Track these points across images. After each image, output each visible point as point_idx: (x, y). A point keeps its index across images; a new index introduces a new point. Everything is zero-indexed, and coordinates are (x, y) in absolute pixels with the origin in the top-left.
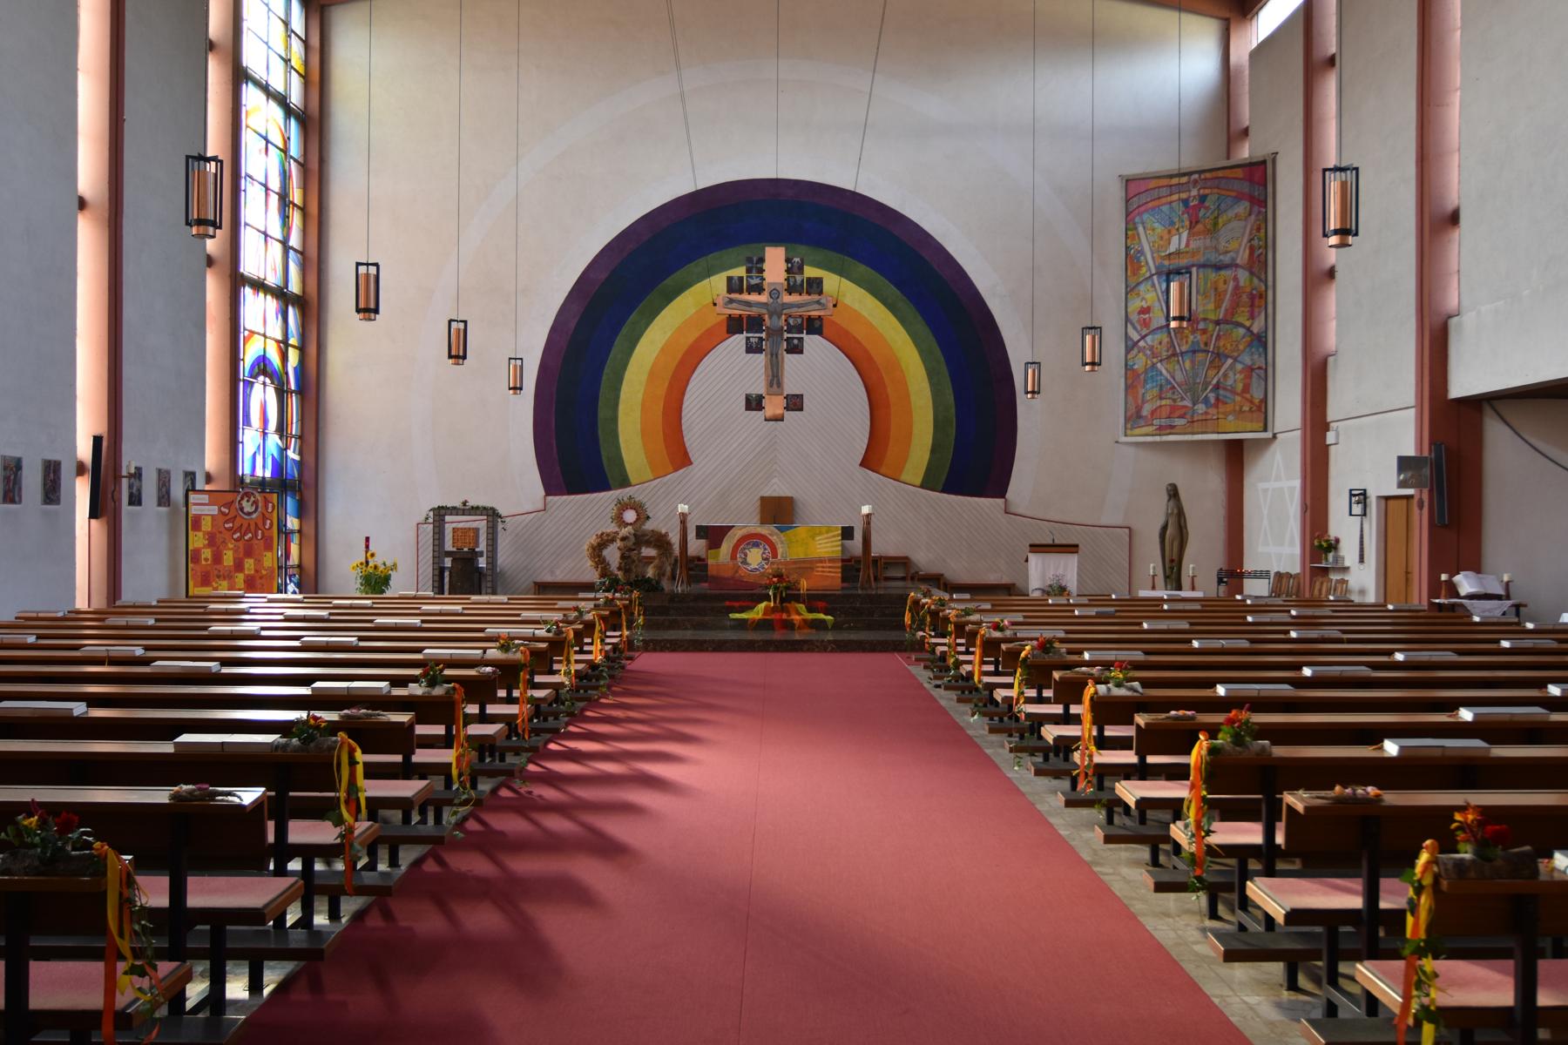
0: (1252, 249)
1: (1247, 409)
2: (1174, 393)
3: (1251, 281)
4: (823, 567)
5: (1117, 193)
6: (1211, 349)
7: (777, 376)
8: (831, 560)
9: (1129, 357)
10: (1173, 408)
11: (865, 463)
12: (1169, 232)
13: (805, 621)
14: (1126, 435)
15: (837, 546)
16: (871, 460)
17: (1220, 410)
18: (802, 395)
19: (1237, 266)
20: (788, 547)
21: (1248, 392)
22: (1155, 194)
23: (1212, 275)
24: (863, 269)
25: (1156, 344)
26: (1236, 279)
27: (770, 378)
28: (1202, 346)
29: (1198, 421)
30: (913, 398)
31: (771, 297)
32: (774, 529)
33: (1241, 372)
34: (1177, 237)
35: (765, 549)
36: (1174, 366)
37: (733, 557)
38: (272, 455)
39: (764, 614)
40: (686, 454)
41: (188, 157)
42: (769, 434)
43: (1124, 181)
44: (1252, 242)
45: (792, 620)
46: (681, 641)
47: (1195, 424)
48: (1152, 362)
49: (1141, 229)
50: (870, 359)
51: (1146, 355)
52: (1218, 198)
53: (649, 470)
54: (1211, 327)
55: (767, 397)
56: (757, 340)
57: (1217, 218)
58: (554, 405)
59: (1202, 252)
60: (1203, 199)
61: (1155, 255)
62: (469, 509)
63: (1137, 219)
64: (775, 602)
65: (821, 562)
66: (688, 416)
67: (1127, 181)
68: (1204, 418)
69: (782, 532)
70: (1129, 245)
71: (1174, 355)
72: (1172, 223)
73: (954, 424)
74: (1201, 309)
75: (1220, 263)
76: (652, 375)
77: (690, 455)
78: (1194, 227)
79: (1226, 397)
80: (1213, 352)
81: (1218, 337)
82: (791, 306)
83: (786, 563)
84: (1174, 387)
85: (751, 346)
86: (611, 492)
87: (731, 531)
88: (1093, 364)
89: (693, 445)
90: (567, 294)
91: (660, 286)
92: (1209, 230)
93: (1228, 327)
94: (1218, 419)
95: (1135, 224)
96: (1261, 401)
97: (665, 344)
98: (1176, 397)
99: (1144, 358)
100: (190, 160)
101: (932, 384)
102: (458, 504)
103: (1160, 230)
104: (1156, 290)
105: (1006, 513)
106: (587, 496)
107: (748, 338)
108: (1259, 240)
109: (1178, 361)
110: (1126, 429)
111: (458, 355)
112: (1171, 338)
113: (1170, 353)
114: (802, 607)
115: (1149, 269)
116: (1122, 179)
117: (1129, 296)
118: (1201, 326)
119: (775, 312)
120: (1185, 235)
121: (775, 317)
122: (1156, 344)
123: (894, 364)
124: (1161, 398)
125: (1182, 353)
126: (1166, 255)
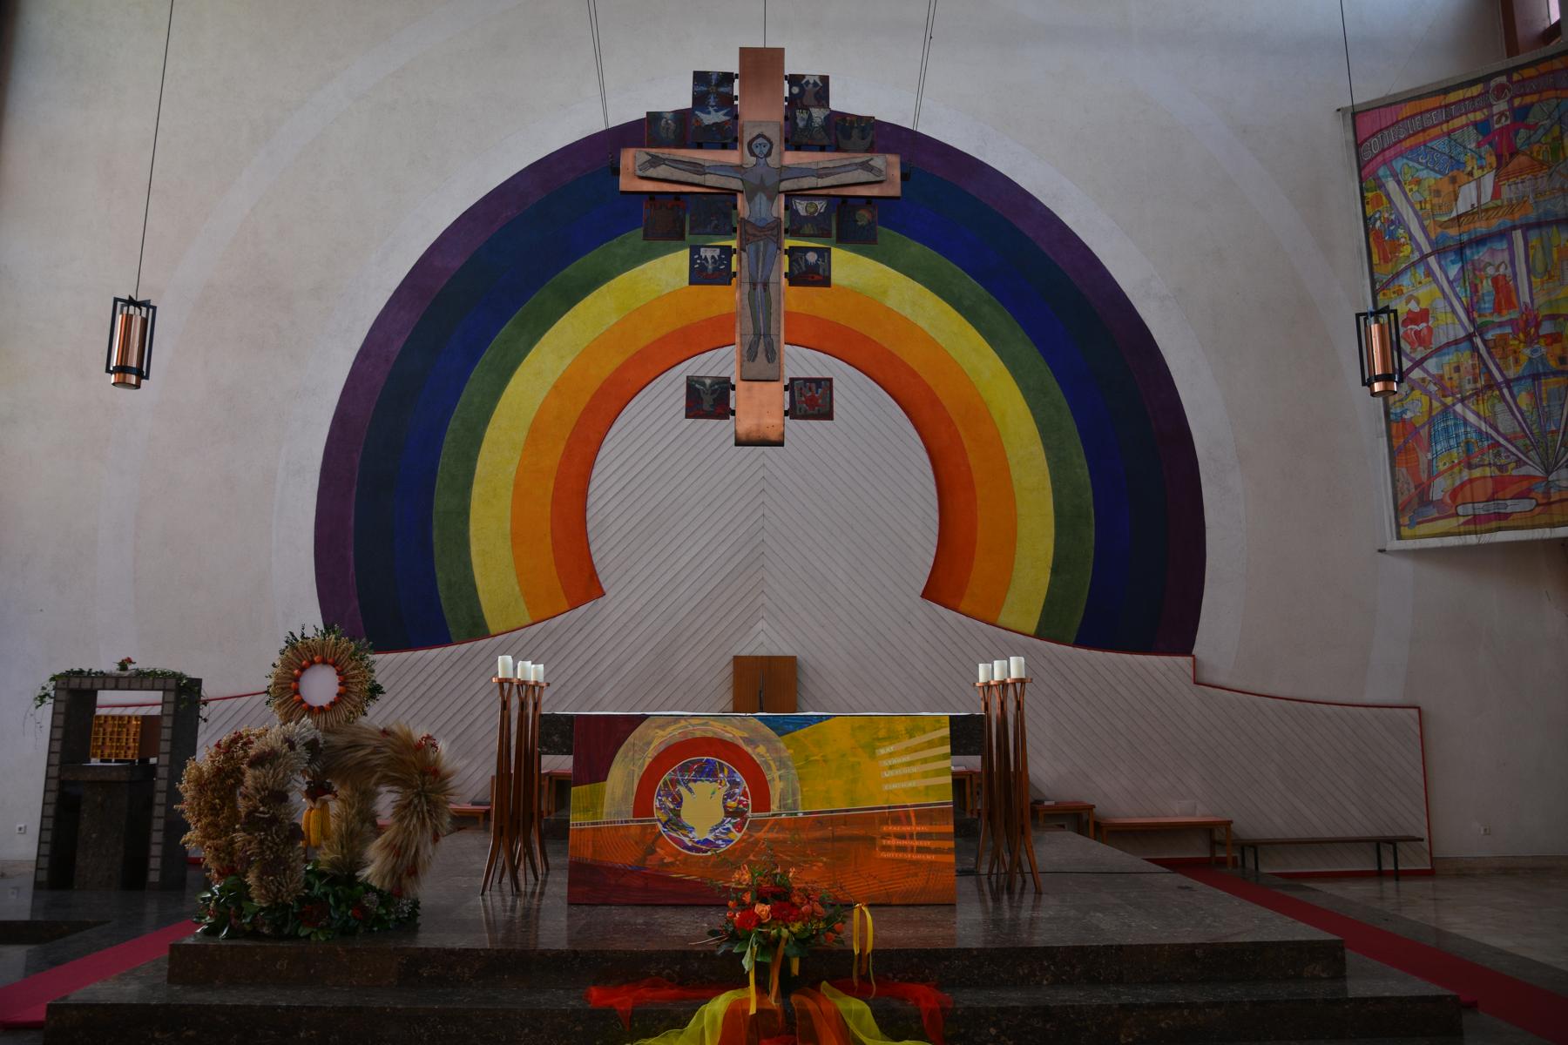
2: (1498, 455)
4: (902, 836)
5: (1337, 137)
7: (767, 335)
10: (1500, 485)
11: (931, 592)
12: (1454, 180)
14: (1399, 537)
15: (939, 773)
18: (830, 380)
20: (801, 779)
24: (916, 249)
28: (1553, 364)
30: (1016, 473)
31: (752, 153)
34: (1473, 185)
35: (734, 784)
36: (1493, 406)
37: (642, 806)
40: (593, 576)
41: (116, 300)
47: (1554, 507)
48: (1444, 404)
49: (1391, 185)
50: (935, 402)
51: (1426, 392)
53: (523, 606)
55: (741, 386)
58: (355, 488)
59: (1531, 201)
60: (1520, 116)
61: (1426, 223)
63: (1381, 172)
64: (762, 988)
65: (896, 820)
67: (1354, 115)
70: (1368, 215)
71: (1491, 385)
72: (1458, 164)
73: (1093, 521)
74: (1540, 300)
76: (536, 432)
77: (601, 578)
78: (1507, 164)
82: (802, 172)
83: (796, 825)
84: (1498, 444)
85: (703, 268)
87: (637, 733)
90: (390, 294)
91: (559, 276)
92: (1542, 164)
95: (1377, 179)
98: (1503, 461)
99: (1425, 399)
100: (119, 304)
101: (1047, 448)
102: (111, 667)
104: (1436, 280)
105: (1196, 683)
106: (405, 655)
109: (1502, 395)
110: (1398, 525)
112: (1480, 356)
113: (1482, 382)
118: (1546, 328)
120: (1488, 181)
121: (761, 199)
123: (979, 413)
124: (1470, 466)
125: (1508, 383)
126: (1452, 220)
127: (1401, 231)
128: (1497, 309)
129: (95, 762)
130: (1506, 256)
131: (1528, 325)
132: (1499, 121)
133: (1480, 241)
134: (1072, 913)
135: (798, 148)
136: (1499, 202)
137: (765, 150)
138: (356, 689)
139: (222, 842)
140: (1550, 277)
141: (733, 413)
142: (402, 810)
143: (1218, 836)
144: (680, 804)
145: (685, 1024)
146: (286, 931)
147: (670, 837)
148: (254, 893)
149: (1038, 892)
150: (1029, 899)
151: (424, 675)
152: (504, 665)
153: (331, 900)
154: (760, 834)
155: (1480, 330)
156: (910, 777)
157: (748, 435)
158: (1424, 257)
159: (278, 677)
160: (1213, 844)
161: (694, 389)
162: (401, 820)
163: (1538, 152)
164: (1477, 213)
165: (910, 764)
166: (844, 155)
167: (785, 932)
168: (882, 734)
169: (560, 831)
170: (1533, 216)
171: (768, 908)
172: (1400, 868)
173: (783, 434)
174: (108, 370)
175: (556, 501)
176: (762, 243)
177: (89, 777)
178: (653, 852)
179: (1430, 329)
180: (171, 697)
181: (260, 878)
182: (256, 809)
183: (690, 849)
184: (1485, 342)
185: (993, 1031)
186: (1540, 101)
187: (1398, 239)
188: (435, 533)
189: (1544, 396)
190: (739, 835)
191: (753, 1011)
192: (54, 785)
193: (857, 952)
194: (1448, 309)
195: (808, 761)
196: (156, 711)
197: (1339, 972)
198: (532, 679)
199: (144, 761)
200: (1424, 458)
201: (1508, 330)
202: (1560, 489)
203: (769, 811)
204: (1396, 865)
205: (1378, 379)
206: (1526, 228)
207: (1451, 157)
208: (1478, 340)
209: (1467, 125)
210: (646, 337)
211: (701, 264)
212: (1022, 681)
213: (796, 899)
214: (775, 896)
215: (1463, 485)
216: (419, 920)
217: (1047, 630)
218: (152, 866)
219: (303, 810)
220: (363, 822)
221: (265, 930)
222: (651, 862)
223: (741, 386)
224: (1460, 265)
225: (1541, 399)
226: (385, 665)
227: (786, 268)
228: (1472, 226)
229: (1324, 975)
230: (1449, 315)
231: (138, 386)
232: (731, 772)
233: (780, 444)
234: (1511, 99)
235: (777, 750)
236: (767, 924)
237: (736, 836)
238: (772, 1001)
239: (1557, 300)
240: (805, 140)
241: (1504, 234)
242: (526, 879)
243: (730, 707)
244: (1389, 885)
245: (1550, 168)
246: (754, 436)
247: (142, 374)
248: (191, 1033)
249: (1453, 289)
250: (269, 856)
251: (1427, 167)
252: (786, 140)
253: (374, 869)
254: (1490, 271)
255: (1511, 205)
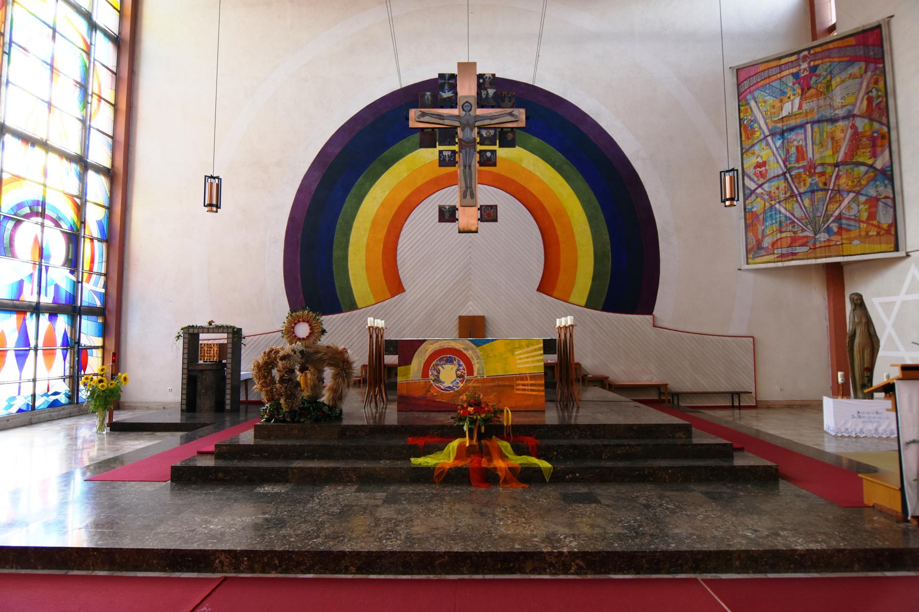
0: (870, 100)
1: (875, 233)
2: (794, 227)
3: (871, 125)
4: (524, 385)
5: (731, 80)
6: (831, 187)
7: (471, 188)
8: (533, 377)
9: (747, 202)
10: (794, 240)
11: (541, 289)
12: (781, 101)
13: (512, 469)
14: (748, 263)
15: (538, 361)
16: (546, 286)
17: (844, 236)
18: (496, 206)
19: (854, 116)
20: (485, 363)
21: (875, 219)
22: (766, 74)
23: (828, 127)
25: (773, 189)
26: (853, 127)
27: (464, 189)
28: (821, 186)
29: (821, 247)
30: (577, 238)
32: (470, 342)
33: (865, 203)
34: (790, 103)
35: (460, 365)
36: (793, 205)
37: (425, 374)
38: (57, 287)
39: (456, 459)
40: (400, 283)
41: (206, 176)
42: (465, 267)
43: (735, 71)
44: (870, 94)
45: (495, 468)
46: (300, 553)
49: (753, 103)
50: (542, 207)
51: (764, 199)
52: (830, 66)
54: (829, 169)
55: (460, 209)
56: (450, 153)
57: (830, 81)
59: (816, 110)
60: (813, 70)
61: (767, 121)
62: (213, 328)
63: (748, 97)
64: (471, 438)
66: (403, 254)
67: (737, 70)
68: (827, 244)
69: (478, 345)
70: (741, 117)
71: (793, 195)
72: (783, 93)
75: (836, 117)
76: (375, 224)
77: (404, 284)
78: (806, 93)
79: (849, 225)
80: (832, 190)
81: (838, 177)
82: (484, 118)
83: (483, 381)
84: (794, 222)
85: (444, 159)
86: (342, 315)
87: (422, 346)
88: (732, 199)
89: (407, 276)
91: (382, 155)
92: (821, 93)
93: (848, 167)
94: (842, 244)
95: (746, 100)
96: (890, 226)
97: (385, 200)
98: (796, 230)
99: (762, 202)
102: (205, 324)
103: (771, 101)
104: (770, 148)
105: (654, 326)
107: (441, 152)
108: (878, 90)
109: (797, 199)
110: (747, 258)
111: (214, 205)
112: (788, 182)
113: (788, 194)
114: (505, 446)
115: (764, 133)
116: (733, 70)
117: (744, 156)
118: (819, 169)
119: (467, 125)
120: (797, 101)
121: (467, 130)
122: (773, 189)
123: (562, 212)
124: (781, 232)
125: (800, 194)
126: (780, 119)
127: (756, 125)
128: (798, 161)
129: (201, 362)
130: (803, 137)
131: (811, 168)
132: (803, 73)
133: (791, 129)
134: (590, 414)
135: (482, 107)
136: (801, 111)
137: (469, 108)
138: (316, 331)
139: (269, 388)
140: (822, 146)
141: (457, 220)
142: (335, 377)
143: (662, 390)
144: (439, 373)
145: (443, 450)
146: (296, 420)
147: (437, 386)
148: (283, 406)
149: (578, 408)
150: (575, 410)
151: (332, 325)
152: (370, 321)
153: (312, 409)
154: (470, 384)
155: (789, 170)
156: (527, 362)
157: (463, 229)
158: (766, 137)
159: (286, 327)
160: (660, 393)
161: (442, 211)
162: (335, 380)
163: (820, 88)
164: (791, 116)
165: (527, 358)
166: (502, 110)
167: (479, 417)
168: (517, 346)
169: (393, 386)
170: (816, 117)
171: (473, 408)
172: (741, 405)
173: (477, 228)
174: (205, 206)
175: (384, 253)
176: (468, 149)
177: (200, 368)
178: (429, 391)
179: (766, 170)
180: (231, 336)
181: (285, 401)
182: (284, 376)
183: (443, 390)
184: (791, 176)
185: (555, 453)
186: (822, 63)
187: (754, 129)
188: (334, 267)
189: (816, 200)
190: (462, 385)
191: (467, 445)
192: (186, 371)
193: (505, 425)
194: (775, 161)
195: (488, 356)
196: (225, 342)
197: (689, 434)
198: (380, 326)
199: (220, 361)
200: (761, 228)
201: (802, 170)
202: (820, 242)
203: (473, 375)
204: (739, 404)
205: (727, 200)
206: (813, 123)
207: (781, 90)
208: (788, 175)
209: (789, 75)
210: (420, 181)
211: (443, 158)
212: (572, 326)
213: (483, 406)
214: (475, 404)
215: (777, 240)
216: (342, 416)
217: (591, 304)
218: (227, 403)
219: (299, 377)
220: (319, 381)
221: (288, 419)
222: (429, 395)
223: (460, 209)
224: (781, 141)
225: (814, 202)
226: (328, 321)
227: (478, 159)
228: (788, 122)
229: (683, 437)
230: (776, 164)
231: (217, 212)
232: (459, 361)
233: (476, 232)
234: (810, 62)
235: (476, 352)
236: (473, 415)
237: (461, 385)
238: (475, 442)
239: (824, 157)
240: (485, 104)
241: (802, 126)
242: (381, 405)
243: (458, 336)
244: (737, 411)
245: (825, 95)
246: (466, 229)
247: (218, 206)
248: (266, 454)
249: (778, 151)
250: (289, 393)
251: (769, 95)
252: (478, 104)
253: (325, 398)
254: (795, 143)
255: (806, 112)
